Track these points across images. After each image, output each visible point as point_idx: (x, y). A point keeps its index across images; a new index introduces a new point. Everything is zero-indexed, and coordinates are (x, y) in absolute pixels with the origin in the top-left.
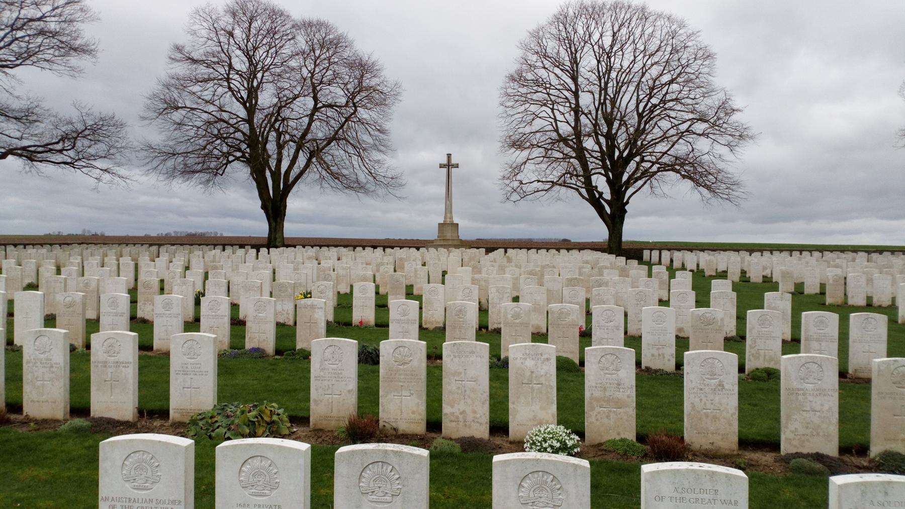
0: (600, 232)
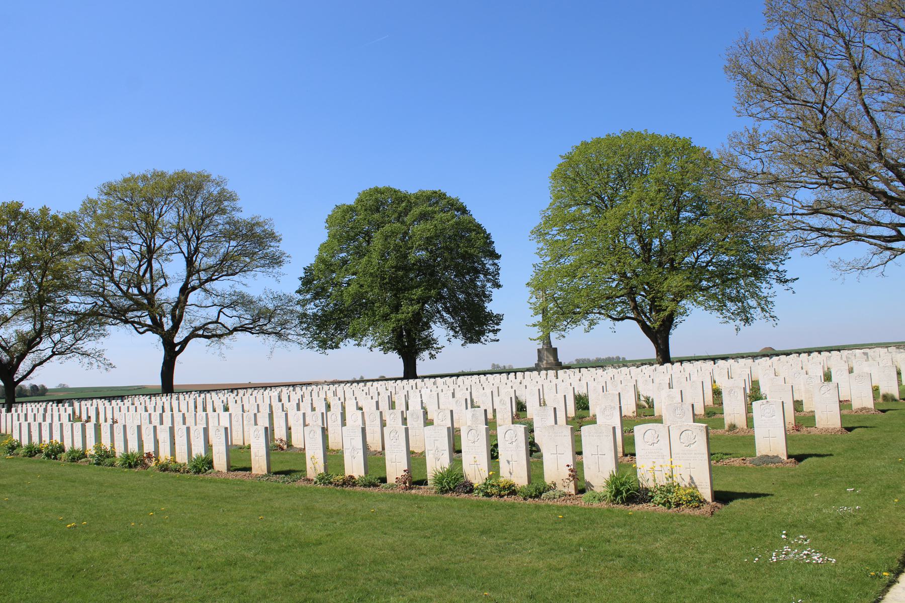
0: (649, 350)
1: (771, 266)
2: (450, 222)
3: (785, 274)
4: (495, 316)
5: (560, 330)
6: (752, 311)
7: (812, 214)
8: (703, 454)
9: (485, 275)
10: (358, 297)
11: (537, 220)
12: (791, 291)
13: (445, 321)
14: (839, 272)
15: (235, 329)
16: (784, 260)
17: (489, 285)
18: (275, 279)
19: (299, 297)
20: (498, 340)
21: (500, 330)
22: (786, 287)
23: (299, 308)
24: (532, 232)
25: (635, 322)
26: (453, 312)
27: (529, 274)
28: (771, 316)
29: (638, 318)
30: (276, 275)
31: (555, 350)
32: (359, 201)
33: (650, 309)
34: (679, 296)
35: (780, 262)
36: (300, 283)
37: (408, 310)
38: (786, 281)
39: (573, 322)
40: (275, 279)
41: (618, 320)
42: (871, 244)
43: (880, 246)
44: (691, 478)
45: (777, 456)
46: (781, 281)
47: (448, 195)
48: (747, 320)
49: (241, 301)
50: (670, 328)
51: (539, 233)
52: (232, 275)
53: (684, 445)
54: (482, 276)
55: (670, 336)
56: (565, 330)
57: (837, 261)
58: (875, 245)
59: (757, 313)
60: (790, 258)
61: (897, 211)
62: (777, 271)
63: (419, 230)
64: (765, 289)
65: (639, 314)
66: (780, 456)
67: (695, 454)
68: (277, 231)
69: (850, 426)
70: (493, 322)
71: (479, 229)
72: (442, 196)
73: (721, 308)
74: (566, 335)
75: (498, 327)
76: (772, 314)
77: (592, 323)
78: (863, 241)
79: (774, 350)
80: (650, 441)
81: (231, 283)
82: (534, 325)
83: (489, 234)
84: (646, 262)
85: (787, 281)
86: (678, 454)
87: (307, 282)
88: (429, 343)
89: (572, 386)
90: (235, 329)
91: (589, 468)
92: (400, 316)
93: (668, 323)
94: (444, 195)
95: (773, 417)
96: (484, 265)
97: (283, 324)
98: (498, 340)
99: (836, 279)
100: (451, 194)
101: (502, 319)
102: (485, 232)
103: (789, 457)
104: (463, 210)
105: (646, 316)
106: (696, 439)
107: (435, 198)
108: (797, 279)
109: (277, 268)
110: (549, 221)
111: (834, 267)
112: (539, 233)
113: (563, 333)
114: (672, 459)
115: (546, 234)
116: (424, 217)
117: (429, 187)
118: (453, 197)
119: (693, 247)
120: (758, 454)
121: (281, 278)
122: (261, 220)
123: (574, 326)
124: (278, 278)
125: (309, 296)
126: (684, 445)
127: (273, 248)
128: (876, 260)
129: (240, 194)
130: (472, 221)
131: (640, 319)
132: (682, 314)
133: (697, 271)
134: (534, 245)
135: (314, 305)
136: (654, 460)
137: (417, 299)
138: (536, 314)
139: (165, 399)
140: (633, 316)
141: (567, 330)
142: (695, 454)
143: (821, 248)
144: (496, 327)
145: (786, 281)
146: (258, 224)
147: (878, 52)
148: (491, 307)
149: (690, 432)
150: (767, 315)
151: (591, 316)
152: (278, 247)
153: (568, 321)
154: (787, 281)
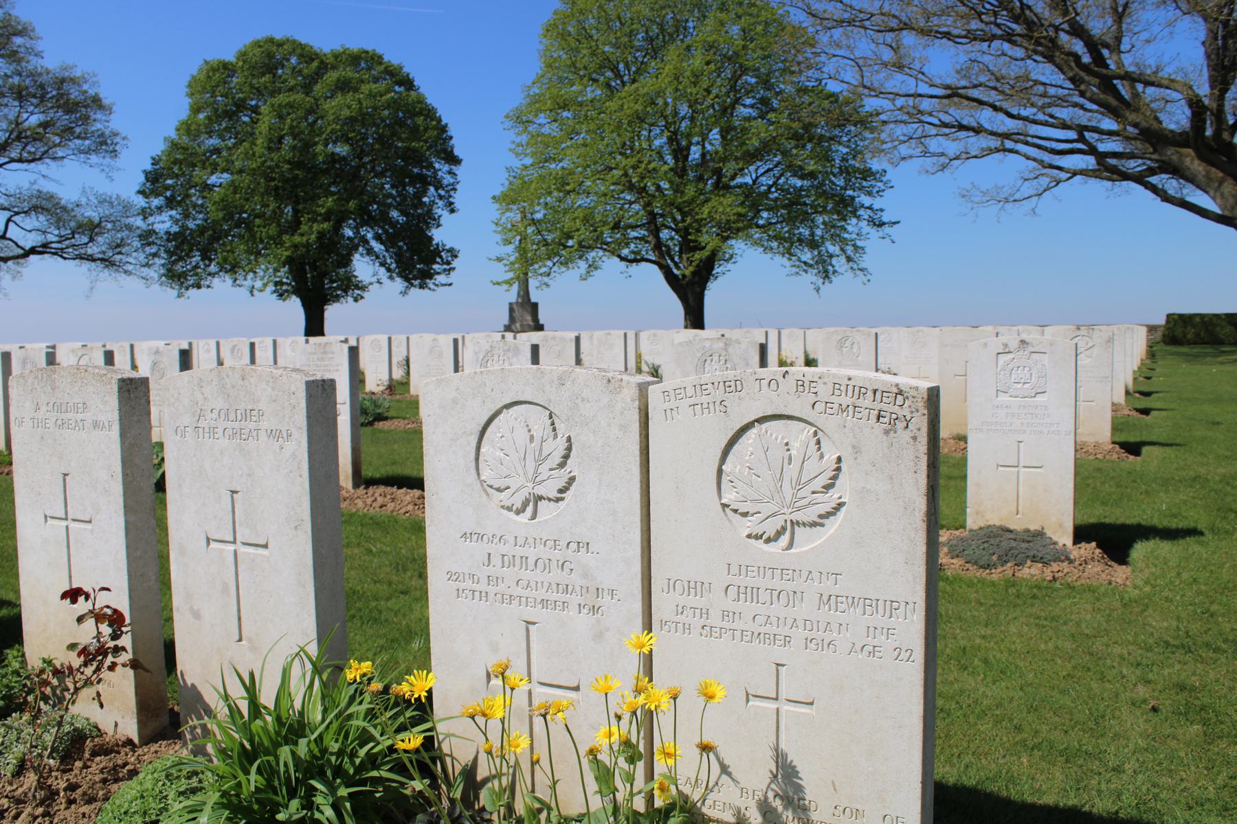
1: (865, 200)
4: (448, 251)
5: (541, 275)
6: (834, 261)
7: (948, 97)
8: (892, 606)
9: (436, 189)
10: (229, 210)
11: (516, 99)
12: (887, 240)
13: (370, 251)
14: (970, 205)
15: (33, 251)
16: (883, 191)
17: (441, 203)
18: (104, 175)
19: (140, 201)
20: (450, 285)
22: (881, 234)
23: (138, 222)
24: (507, 117)
25: (655, 268)
26: (389, 241)
27: (499, 184)
28: (859, 269)
29: (661, 261)
30: (107, 170)
31: (535, 307)
32: (243, 55)
33: (681, 252)
34: (728, 230)
35: (877, 192)
36: (142, 178)
37: (310, 232)
38: (881, 224)
39: (561, 263)
40: (104, 175)
41: (631, 261)
42: (1028, 158)
43: (1041, 162)
44: (786, 773)
45: (1040, 534)
46: (875, 224)
47: (386, 59)
48: (826, 275)
49: (43, 205)
50: (707, 280)
51: (520, 119)
52: (29, 161)
53: (749, 525)
54: (432, 189)
55: (706, 292)
56: (549, 275)
58: (1034, 160)
59: (839, 263)
60: (892, 187)
61: (1088, 95)
62: (870, 208)
63: (337, 107)
64: (852, 225)
65: (662, 255)
66: (1049, 533)
67: (826, 600)
68: (107, 97)
71: (429, 113)
72: (374, 59)
73: (789, 253)
74: (550, 282)
76: (862, 265)
77: (593, 267)
78: (1017, 152)
80: (514, 483)
81: (33, 177)
82: (499, 259)
83: (446, 125)
84: (676, 173)
85: (884, 224)
86: (694, 587)
87: (154, 181)
88: (350, 286)
90: (33, 251)
91: (197, 615)
92: (297, 239)
93: (704, 272)
94: (380, 57)
95: (1039, 398)
96: (436, 171)
97: (118, 246)
98: (450, 285)
99: (965, 215)
100: (392, 57)
101: (456, 256)
102: (439, 120)
103: (1082, 534)
104: (408, 83)
105: (672, 260)
106: (844, 489)
107: (365, 61)
108: (898, 222)
109: (109, 160)
110: (535, 103)
111: (963, 196)
112: (520, 119)
113: (546, 279)
114: (654, 641)
115: (527, 122)
116: (344, 86)
117: (355, 44)
119: (752, 157)
120: (972, 522)
121: (115, 175)
122: (77, 73)
123: (563, 269)
124: (110, 174)
125: (156, 202)
126: (749, 525)
127: (99, 123)
128: (1028, 188)
129: (39, 31)
130: (421, 100)
131: (664, 263)
132: (727, 261)
133: (753, 199)
134: (512, 136)
136: (531, 613)
137: (325, 213)
138: (507, 242)
140: (654, 258)
141: (552, 275)
142: (826, 600)
143: (951, 160)
146: (73, 80)
148: (438, 235)
149: (799, 436)
150: (855, 266)
151: (592, 255)
152: (108, 122)
153: (555, 260)
154: (884, 224)
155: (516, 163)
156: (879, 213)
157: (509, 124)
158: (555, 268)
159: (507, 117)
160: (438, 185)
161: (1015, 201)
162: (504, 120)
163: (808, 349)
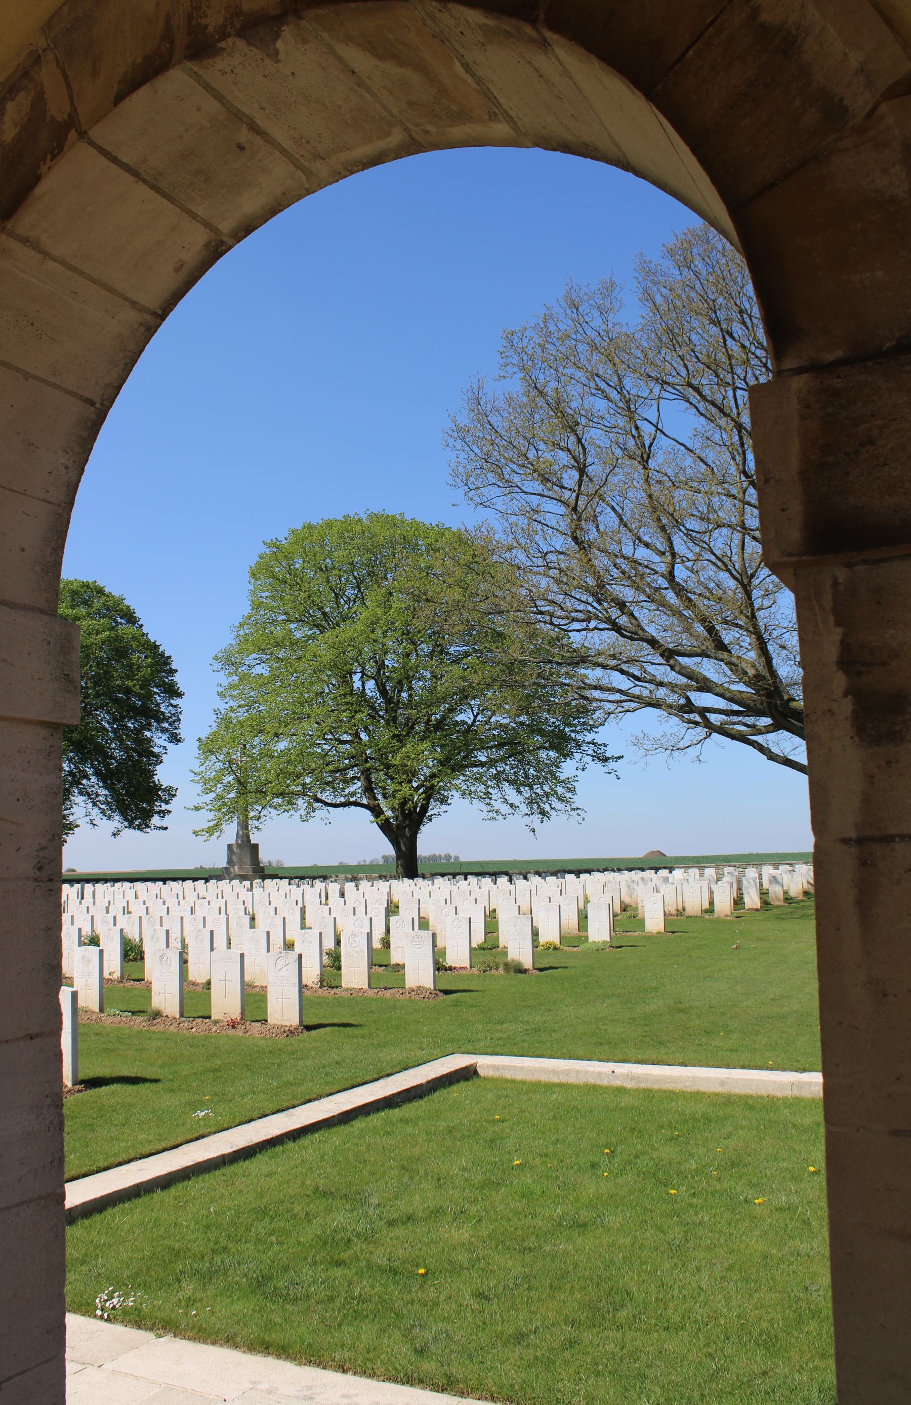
2: (100, 636)
3: (605, 748)
11: (227, 639)
20: (166, 828)
21: (169, 812)
22: (606, 770)
24: (216, 658)
26: (106, 778)
31: (255, 847)
38: (606, 760)
51: (229, 661)
57: (641, 735)
61: (677, 669)
69: (448, 988)
70: (161, 799)
74: (261, 826)
75: (168, 807)
79: (665, 855)
83: (169, 657)
89: (90, 914)
98: (166, 828)
100: (113, 588)
101: (174, 796)
104: (131, 618)
108: (622, 757)
110: (246, 644)
112: (229, 661)
118: (116, 593)
135: (547, 755)
139: (403, 888)
144: (164, 807)
145: (606, 760)
147: (51, 384)
155: (223, 707)
156: (602, 747)
157: (217, 665)
158: (264, 812)
159: (216, 658)
160: (159, 717)
161: (679, 749)
162: (212, 661)
163: (587, 892)
